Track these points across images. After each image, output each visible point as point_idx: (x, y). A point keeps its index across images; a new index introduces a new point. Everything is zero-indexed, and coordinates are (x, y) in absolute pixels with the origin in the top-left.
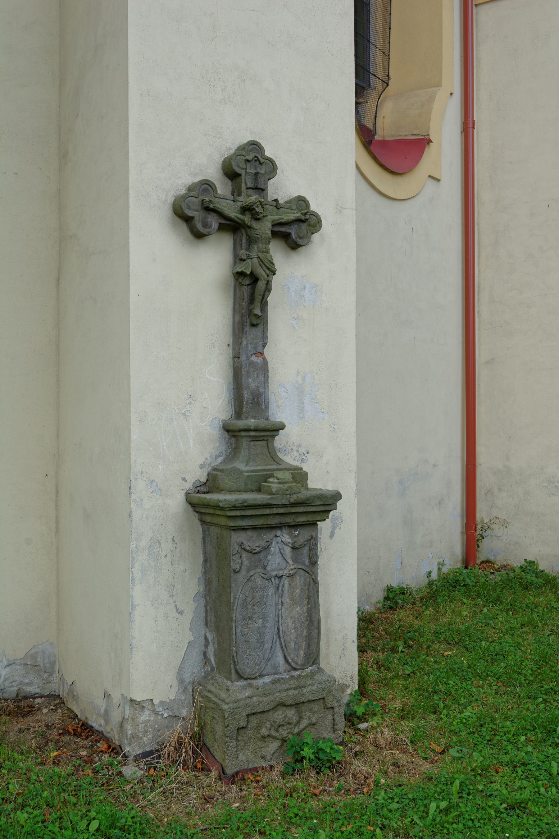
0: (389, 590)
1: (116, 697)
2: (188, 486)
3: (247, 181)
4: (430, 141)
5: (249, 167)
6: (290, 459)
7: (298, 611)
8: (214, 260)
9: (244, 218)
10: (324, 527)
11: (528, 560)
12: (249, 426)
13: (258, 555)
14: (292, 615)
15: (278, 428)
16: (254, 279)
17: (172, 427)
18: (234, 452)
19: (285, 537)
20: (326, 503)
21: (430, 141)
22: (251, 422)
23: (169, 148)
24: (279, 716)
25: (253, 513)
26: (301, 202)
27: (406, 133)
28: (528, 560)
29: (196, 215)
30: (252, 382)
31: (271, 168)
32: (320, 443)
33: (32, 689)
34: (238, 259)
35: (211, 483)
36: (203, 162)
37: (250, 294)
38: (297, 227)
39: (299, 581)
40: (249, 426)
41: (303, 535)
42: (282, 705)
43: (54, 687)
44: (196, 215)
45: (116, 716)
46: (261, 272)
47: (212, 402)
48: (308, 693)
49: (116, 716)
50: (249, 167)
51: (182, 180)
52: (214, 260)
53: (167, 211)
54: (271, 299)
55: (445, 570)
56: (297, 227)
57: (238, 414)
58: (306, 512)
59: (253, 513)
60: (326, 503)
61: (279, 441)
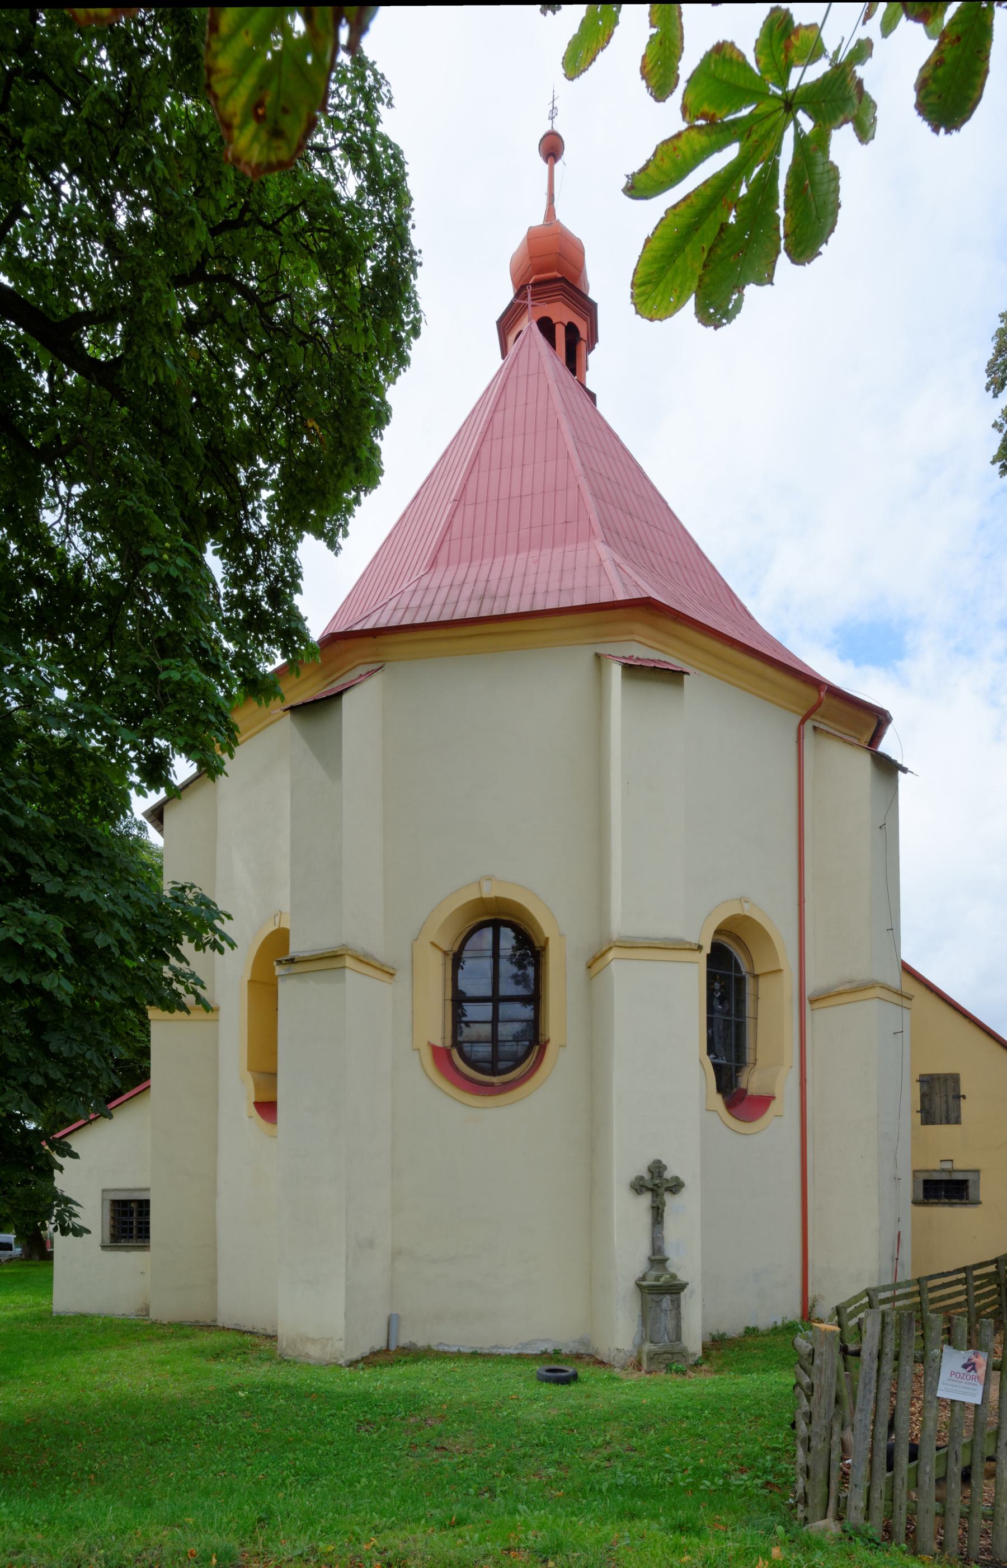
0: (747, 1328)
1: (612, 1349)
2: (636, 1278)
3: (656, 1174)
4: (774, 1098)
5: (657, 1168)
6: (672, 1270)
7: (673, 1322)
8: (646, 1200)
9: (657, 1186)
10: (682, 1294)
11: (85, 1235)
12: (658, 1259)
13: (658, 1303)
14: (670, 1324)
15: (666, 1260)
16: (658, 1208)
17: (629, 1257)
18: (651, 1268)
19: (668, 1297)
20: (683, 1287)
21: (774, 1098)
22: (658, 1257)
23: (627, 1163)
24: (665, 1356)
25: (660, 1290)
26: (677, 1179)
27: (763, 1092)
28: (85, 1235)
29: (639, 1187)
30: (658, 1243)
31: (665, 1168)
32: (686, 1262)
33: (582, 1352)
34: (653, 1202)
35: (643, 1278)
36: (640, 1168)
37: (657, 1214)
38: (676, 1186)
39: (673, 1312)
40: (658, 1259)
41: (675, 1297)
42: (665, 1352)
43: (590, 1351)
44: (639, 1187)
45: (612, 1356)
46: (660, 1206)
47: (644, 1249)
48: (676, 1350)
49: (612, 1356)
50: (657, 1168)
51: (632, 1175)
52: (646, 1200)
53: (628, 1186)
54: (665, 1214)
55: (786, 1322)
56: (676, 1186)
57: (654, 1254)
58: (675, 1289)
59: (660, 1290)
60: (683, 1287)
61: (668, 1263)
